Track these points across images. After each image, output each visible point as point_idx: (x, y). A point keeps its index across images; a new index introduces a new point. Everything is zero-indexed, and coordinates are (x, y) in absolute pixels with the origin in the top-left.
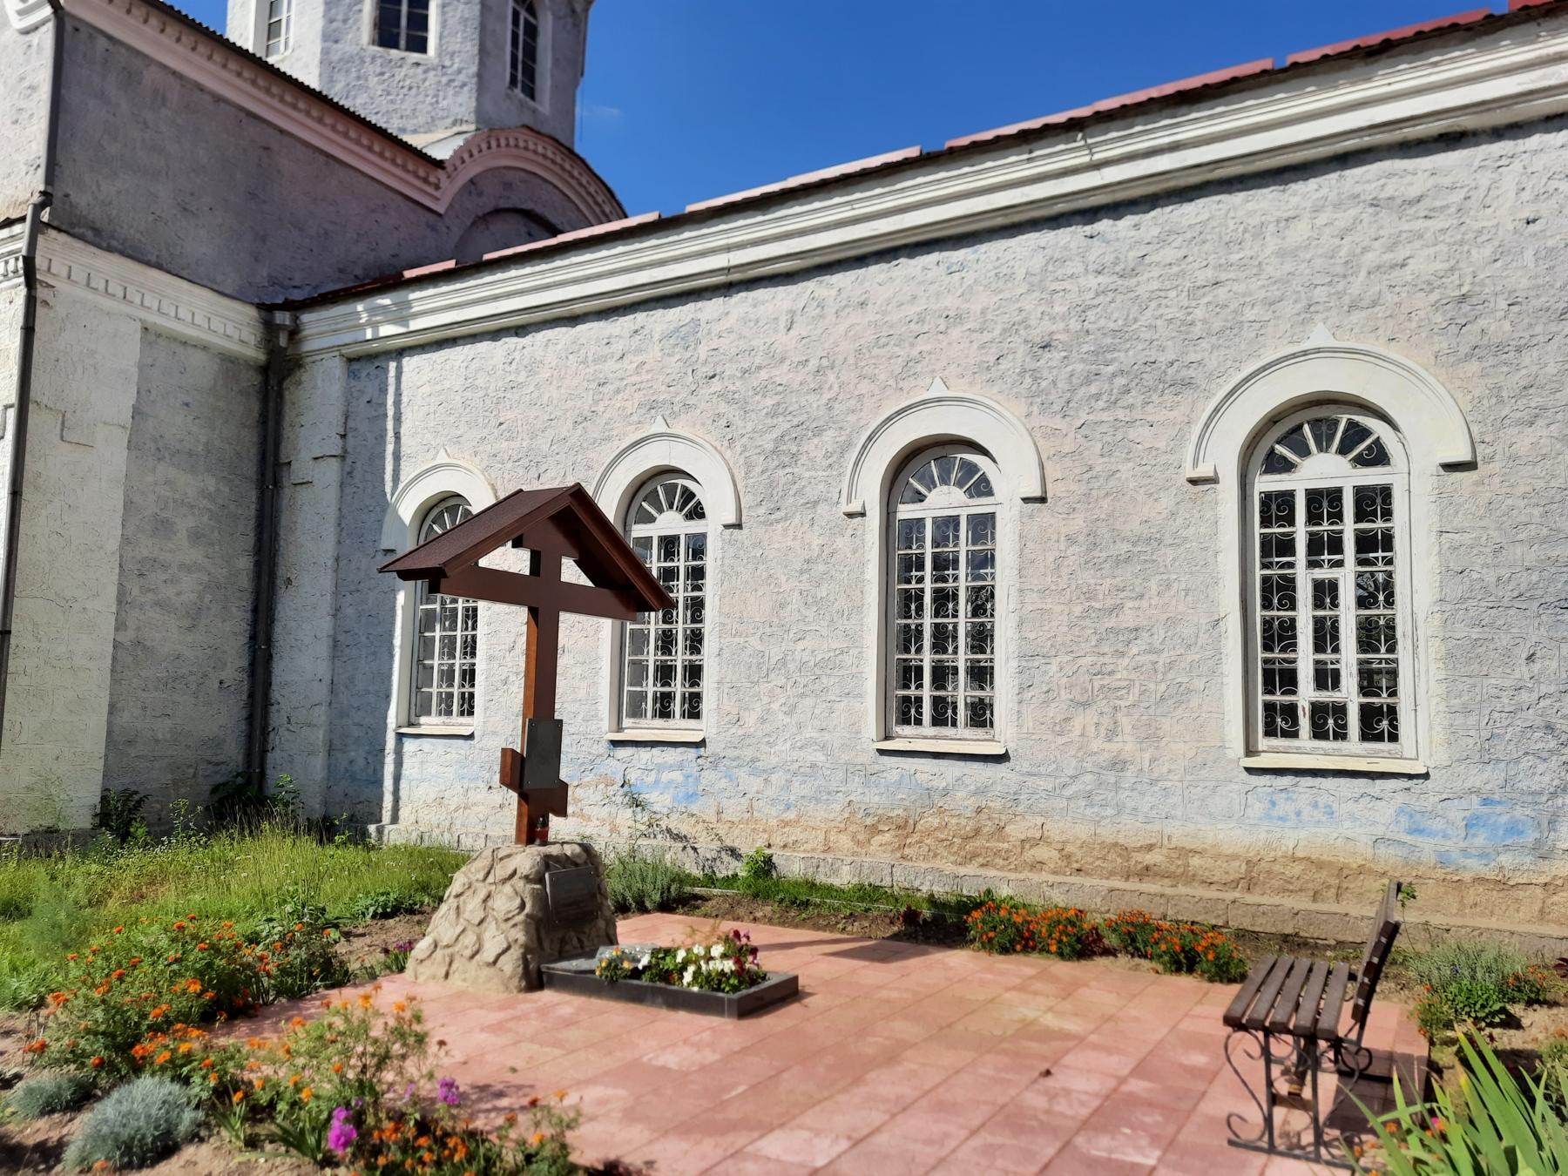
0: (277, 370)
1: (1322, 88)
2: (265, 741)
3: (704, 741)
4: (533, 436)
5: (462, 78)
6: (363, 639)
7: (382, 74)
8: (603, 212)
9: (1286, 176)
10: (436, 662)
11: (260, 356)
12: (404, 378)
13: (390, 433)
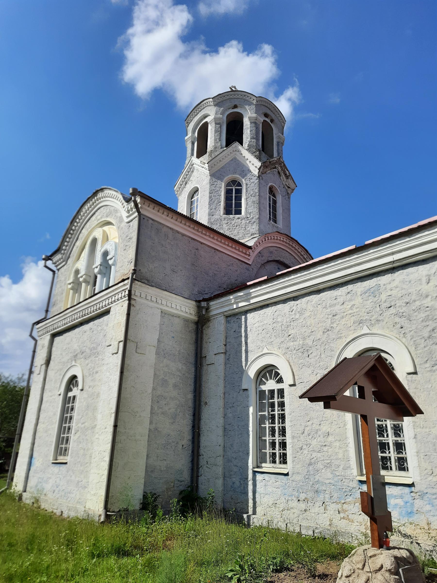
0: (201, 322)
1: (429, 231)
2: (198, 472)
3: (413, 483)
4: (304, 339)
5: (254, 220)
6: (236, 427)
7: (228, 223)
8: (304, 258)
9: (381, 274)
10: (267, 438)
11: (195, 318)
12: (248, 321)
13: (244, 342)
